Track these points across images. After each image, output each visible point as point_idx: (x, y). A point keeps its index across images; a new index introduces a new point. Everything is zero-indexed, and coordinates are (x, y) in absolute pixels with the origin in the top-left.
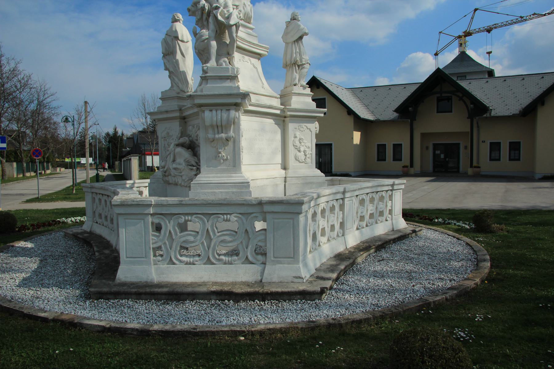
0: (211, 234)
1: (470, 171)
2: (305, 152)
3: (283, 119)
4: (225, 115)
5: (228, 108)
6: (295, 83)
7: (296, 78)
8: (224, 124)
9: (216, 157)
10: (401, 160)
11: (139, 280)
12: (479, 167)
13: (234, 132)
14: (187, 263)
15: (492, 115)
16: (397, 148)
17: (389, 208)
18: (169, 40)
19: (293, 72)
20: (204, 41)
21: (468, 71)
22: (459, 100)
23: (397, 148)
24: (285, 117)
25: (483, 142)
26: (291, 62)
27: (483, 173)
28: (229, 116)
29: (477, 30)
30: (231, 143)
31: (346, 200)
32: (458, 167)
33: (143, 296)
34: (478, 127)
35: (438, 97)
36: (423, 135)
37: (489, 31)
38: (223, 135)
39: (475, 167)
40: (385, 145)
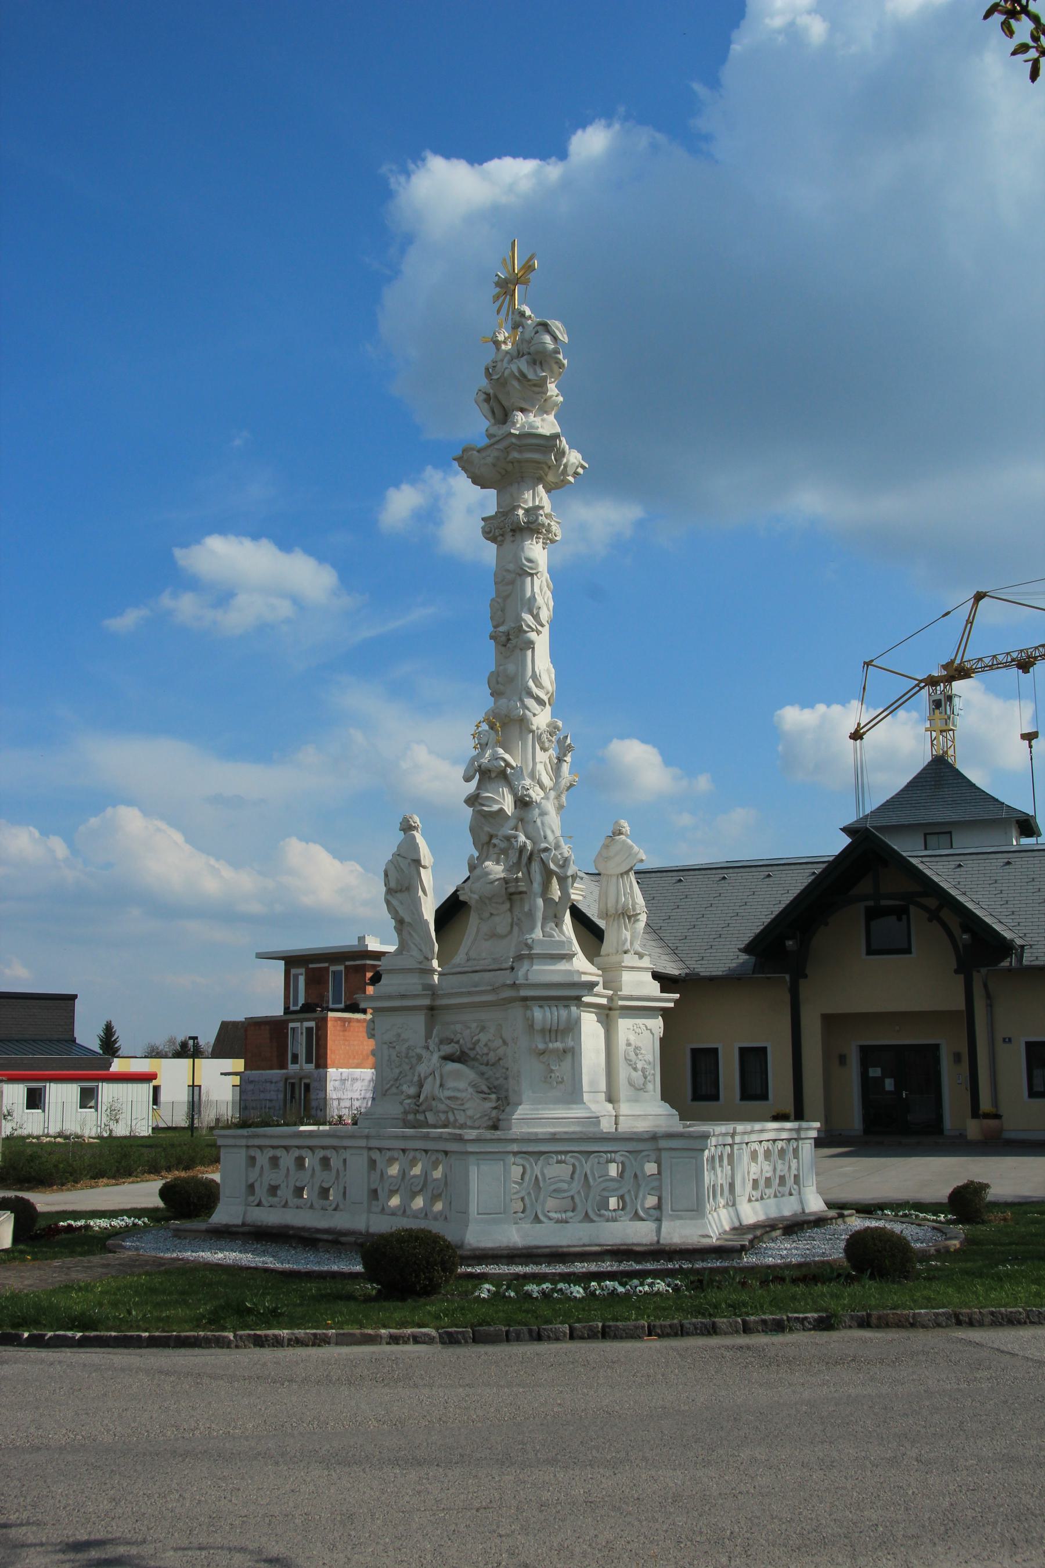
0: (591, 1180)
1: (973, 1129)
2: (643, 1070)
3: (607, 1012)
4: (564, 1013)
5: (566, 1003)
6: (625, 948)
7: (626, 939)
8: (561, 1027)
9: (546, 1078)
10: (764, 1097)
11: (497, 1245)
12: (997, 1116)
13: (573, 1040)
14: (558, 1221)
15: (1025, 962)
16: (753, 1060)
17: (794, 1172)
18: (404, 864)
19: (619, 927)
20: (492, 883)
21: (955, 818)
22: (930, 920)
23: (753, 1060)
24: (610, 1009)
25: (1008, 1040)
26: (617, 911)
27: (1012, 1135)
28: (570, 1012)
29: (987, 661)
30: (569, 1057)
31: (736, 1147)
32: (940, 1118)
33: (517, 1260)
34: (988, 996)
35: (867, 908)
36: (830, 1021)
37: (1025, 665)
38: (558, 1045)
39: (987, 1116)
40: (716, 1050)
